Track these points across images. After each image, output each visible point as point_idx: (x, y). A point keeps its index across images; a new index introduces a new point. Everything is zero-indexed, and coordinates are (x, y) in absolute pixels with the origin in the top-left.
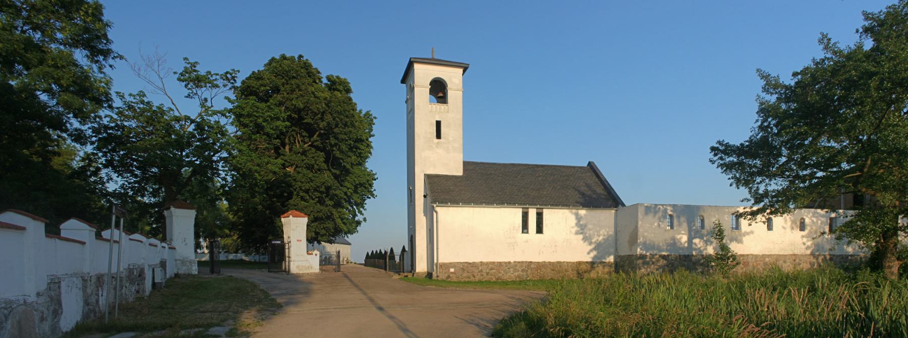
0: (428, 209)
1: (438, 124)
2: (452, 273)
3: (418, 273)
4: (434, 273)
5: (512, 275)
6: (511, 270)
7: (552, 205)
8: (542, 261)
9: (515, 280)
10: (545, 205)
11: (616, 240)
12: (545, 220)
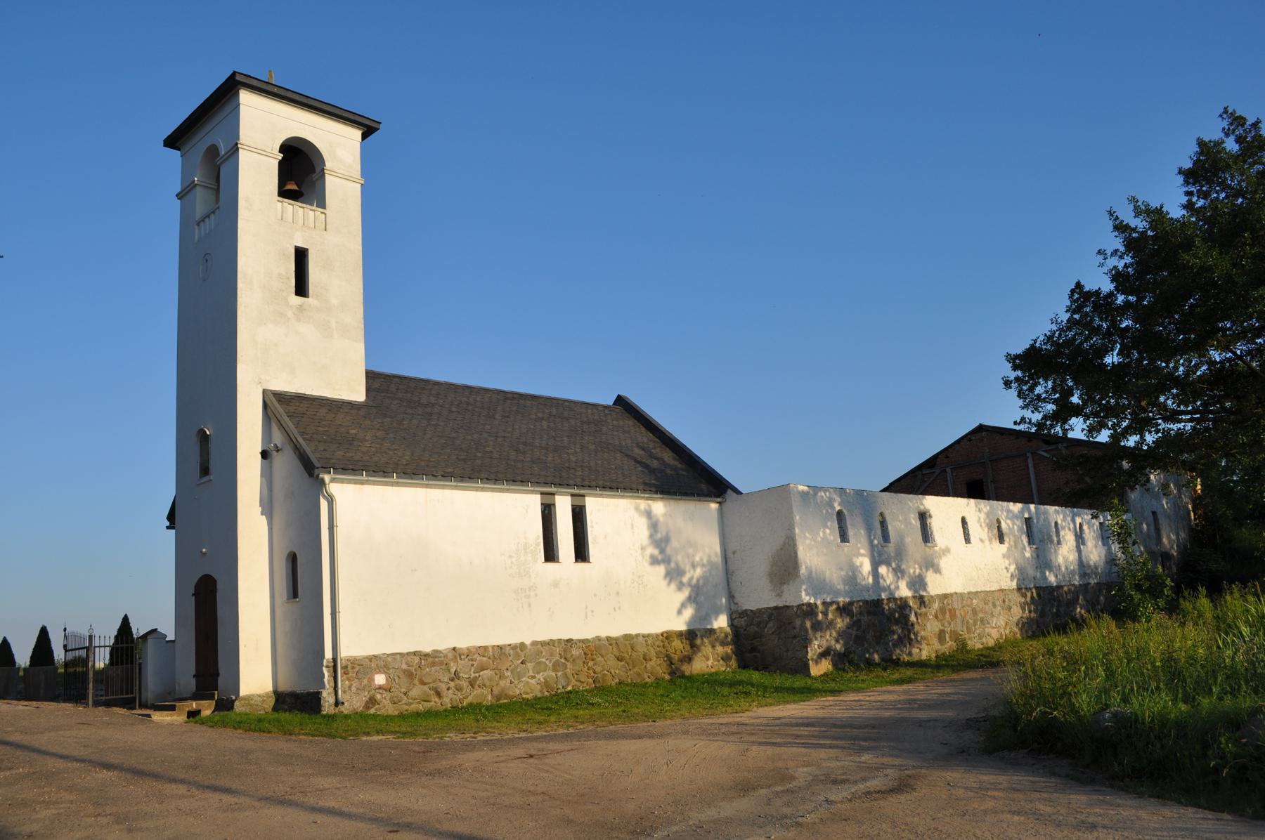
0: (442, 483)
1: (301, 256)
2: (380, 687)
3: (244, 698)
4: (325, 694)
5: (533, 681)
6: (530, 666)
7: (604, 488)
8: (594, 636)
9: (539, 695)
10: (590, 487)
11: (728, 573)
12: (592, 527)
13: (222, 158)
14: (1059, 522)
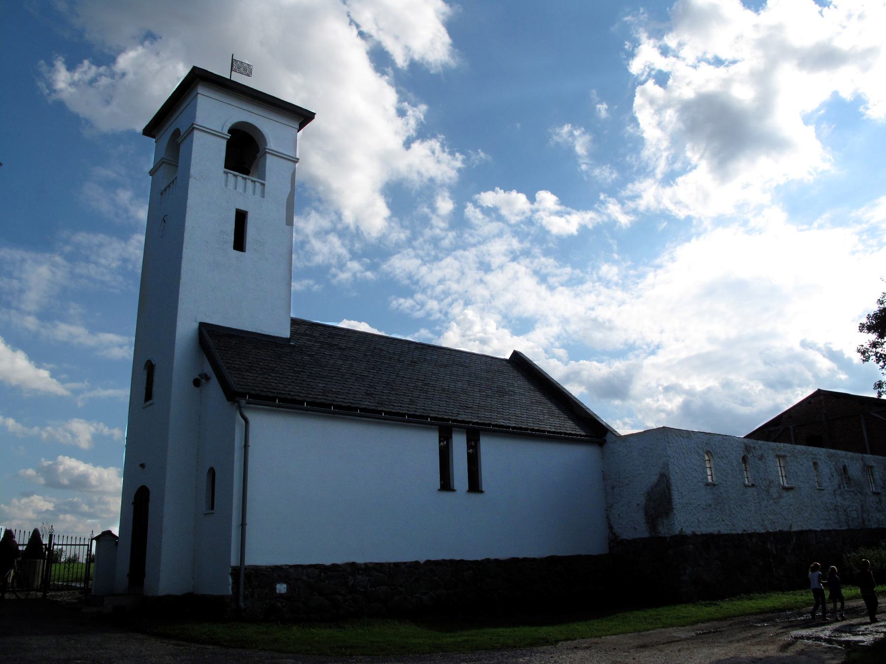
1: (241, 217)
13: (182, 136)
14: (824, 492)
